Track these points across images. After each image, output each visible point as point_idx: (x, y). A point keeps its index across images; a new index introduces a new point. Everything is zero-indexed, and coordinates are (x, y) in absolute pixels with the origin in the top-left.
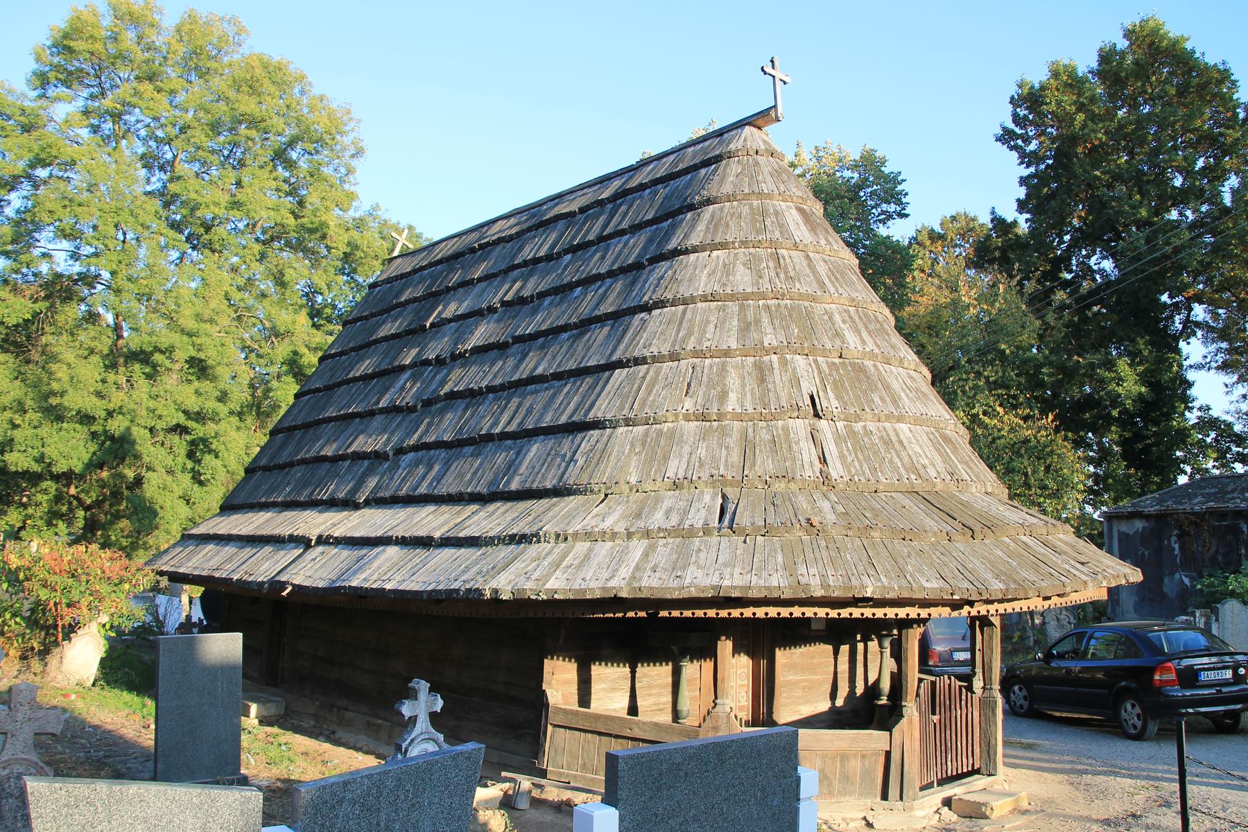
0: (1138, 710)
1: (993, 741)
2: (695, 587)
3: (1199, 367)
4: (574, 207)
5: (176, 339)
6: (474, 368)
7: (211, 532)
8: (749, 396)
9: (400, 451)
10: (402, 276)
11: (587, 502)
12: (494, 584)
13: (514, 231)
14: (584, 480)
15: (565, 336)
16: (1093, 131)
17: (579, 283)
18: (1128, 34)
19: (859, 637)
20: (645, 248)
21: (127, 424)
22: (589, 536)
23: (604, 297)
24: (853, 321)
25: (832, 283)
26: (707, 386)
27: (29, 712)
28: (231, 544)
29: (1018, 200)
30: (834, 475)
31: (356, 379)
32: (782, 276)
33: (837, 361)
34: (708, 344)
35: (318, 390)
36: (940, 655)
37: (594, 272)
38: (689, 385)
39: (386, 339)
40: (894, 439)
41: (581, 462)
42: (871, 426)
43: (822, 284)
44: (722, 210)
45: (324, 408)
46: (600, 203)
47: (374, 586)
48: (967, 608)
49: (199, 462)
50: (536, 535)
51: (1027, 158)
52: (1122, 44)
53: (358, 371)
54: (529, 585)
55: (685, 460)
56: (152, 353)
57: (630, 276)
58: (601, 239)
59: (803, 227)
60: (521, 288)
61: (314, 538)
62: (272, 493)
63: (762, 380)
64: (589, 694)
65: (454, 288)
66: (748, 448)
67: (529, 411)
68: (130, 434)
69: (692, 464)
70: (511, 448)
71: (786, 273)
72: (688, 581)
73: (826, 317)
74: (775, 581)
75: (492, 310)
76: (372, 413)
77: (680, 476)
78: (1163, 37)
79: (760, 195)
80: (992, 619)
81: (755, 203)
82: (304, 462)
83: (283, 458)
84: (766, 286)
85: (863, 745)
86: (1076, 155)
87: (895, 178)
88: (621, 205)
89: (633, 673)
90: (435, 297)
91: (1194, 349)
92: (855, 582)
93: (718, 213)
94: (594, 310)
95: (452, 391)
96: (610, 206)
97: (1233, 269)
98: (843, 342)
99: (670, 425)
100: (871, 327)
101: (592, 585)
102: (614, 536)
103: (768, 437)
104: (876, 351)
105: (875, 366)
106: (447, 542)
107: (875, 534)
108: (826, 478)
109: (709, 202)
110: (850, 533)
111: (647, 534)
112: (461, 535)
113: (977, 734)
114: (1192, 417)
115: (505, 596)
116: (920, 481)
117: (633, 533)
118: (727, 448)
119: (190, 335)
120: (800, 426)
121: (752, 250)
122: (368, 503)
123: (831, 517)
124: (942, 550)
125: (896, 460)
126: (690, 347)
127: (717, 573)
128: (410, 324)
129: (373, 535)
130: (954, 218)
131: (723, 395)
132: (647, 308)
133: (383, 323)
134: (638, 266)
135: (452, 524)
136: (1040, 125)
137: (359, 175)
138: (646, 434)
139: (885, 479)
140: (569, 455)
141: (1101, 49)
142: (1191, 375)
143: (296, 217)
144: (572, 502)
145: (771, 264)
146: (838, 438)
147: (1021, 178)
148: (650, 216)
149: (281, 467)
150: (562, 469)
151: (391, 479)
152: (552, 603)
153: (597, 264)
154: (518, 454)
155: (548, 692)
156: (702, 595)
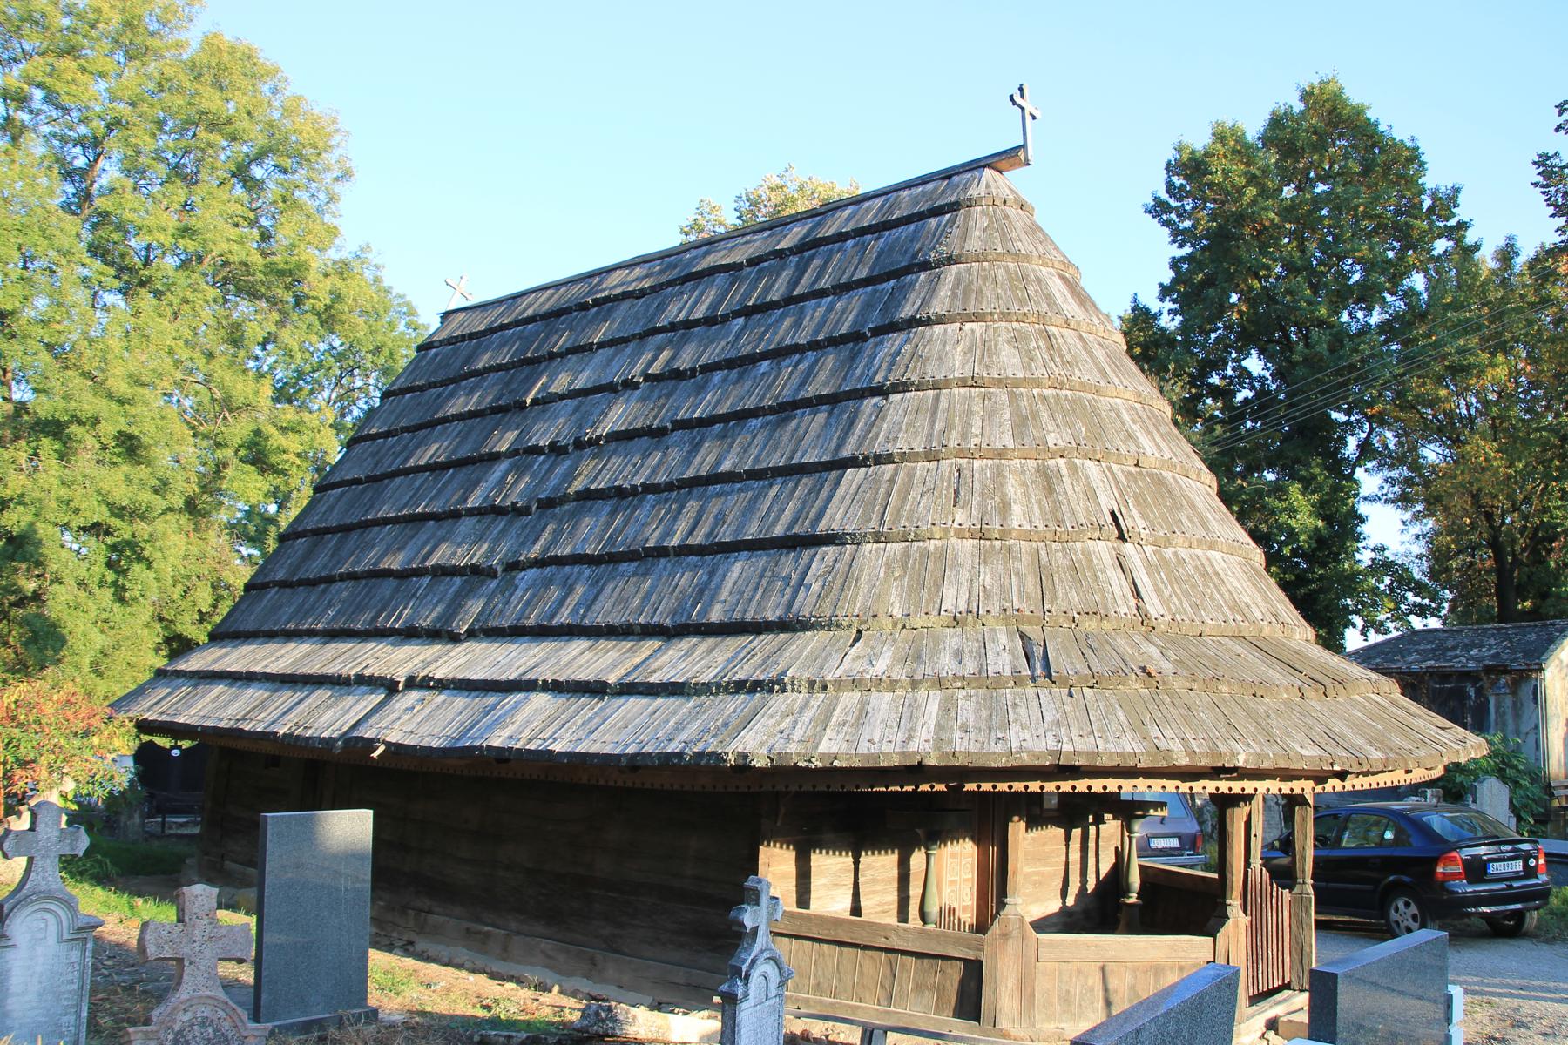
0: (1414, 909)
1: (1307, 949)
2: (1028, 752)
3: (1374, 499)
4: (739, 256)
5: (101, 406)
6: (616, 461)
7: (217, 667)
9: (513, 566)
10: (472, 336)
13: (646, 284)
14: (826, 610)
16: (1265, 209)
17: (764, 356)
18: (1306, 96)
19: (1091, 819)
20: (861, 314)
21: (30, 518)
22: (857, 684)
23: (808, 376)
26: (982, 494)
27: (209, 929)
28: (254, 684)
29: (1161, 285)
30: (1153, 613)
31: (418, 469)
32: (1057, 359)
33: (1133, 469)
34: (977, 440)
35: (357, 482)
37: (787, 342)
38: (957, 492)
39: (460, 417)
41: (816, 587)
42: (1183, 553)
43: (1103, 373)
44: (969, 270)
46: (780, 254)
47: (532, 746)
49: (125, 572)
51: (1179, 237)
52: (1298, 107)
53: (425, 456)
54: (792, 748)
55: (965, 588)
56: (67, 424)
58: (789, 300)
60: (673, 358)
62: (305, 617)
63: (1050, 490)
64: (808, 892)
66: (1043, 574)
67: (720, 519)
68: (35, 532)
69: (975, 593)
70: (696, 567)
71: (1061, 356)
72: (1015, 744)
75: (629, 385)
76: (455, 515)
77: (962, 607)
78: (1345, 104)
79: (1016, 255)
81: (1011, 265)
82: (352, 576)
83: (314, 569)
84: (1040, 372)
85: (1182, 954)
88: (812, 258)
89: (856, 863)
91: (1369, 480)
92: (1223, 748)
97: (1424, 384)
99: (938, 543)
100: (1162, 429)
101: (887, 748)
102: (893, 685)
103: (1067, 562)
106: (628, 689)
107: (1224, 688)
109: (950, 260)
111: (939, 683)
112: (652, 680)
113: (1287, 940)
114: (1365, 558)
115: (759, 763)
117: (920, 682)
118: (1018, 574)
119: (121, 402)
120: (1103, 550)
121: (1015, 325)
122: (471, 634)
125: (1217, 596)
126: (953, 444)
127: (1050, 735)
129: (503, 678)
131: (1005, 507)
132: (882, 391)
133: (452, 395)
135: (628, 665)
137: (343, 206)
138: (906, 553)
139: (1211, 620)
140: (795, 578)
141: (1274, 112)
142: (1363, 508)
143: (264, 254)
144: (809, 642)
145: (1042, 344)
146: (1150, 568)
148: (863, 274)
149: (311, 583)
150: (787, 597)
151: (507, 602)
152: (830, 772)
153: (784, 331)
154: (712, 574)
156: (1037, 763)
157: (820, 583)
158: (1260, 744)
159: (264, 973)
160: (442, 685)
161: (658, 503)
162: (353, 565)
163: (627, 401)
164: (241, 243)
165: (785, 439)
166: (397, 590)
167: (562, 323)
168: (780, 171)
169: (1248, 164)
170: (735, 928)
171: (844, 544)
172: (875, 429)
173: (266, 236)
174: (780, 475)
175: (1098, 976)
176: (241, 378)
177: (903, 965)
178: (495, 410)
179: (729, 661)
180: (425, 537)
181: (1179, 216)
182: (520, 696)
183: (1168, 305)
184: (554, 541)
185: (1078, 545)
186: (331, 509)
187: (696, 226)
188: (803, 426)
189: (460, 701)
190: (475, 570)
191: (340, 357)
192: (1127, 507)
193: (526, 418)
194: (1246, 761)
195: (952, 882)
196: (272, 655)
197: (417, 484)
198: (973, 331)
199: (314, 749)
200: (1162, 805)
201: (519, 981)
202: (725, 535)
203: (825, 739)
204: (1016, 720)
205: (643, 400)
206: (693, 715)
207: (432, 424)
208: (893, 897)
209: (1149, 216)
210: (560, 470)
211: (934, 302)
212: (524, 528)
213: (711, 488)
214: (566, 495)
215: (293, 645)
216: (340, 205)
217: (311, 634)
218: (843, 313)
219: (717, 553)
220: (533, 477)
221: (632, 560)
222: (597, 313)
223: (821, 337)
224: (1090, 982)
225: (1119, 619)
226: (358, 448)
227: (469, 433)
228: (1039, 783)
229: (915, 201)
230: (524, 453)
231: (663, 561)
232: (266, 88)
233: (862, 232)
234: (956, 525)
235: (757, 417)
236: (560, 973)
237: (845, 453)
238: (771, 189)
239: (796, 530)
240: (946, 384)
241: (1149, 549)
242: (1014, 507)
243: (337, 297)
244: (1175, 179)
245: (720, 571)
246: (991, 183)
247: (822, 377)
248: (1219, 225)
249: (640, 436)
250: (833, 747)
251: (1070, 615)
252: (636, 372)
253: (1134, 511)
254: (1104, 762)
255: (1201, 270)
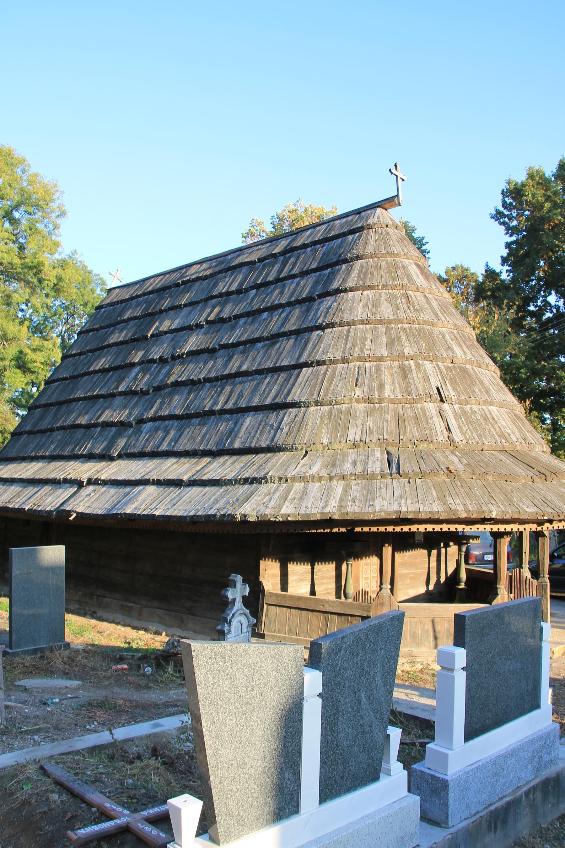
1: (545, 610)
2: (384, 512)
6: (191, 366)
8: (398, 387)
9: (141, 421)
10: (122, 301)
11: (293, 457)
12: (242, 511)
13: (208, 273)
14: (290, 441)
15: (260, 345)
19: (442, 545)
22: (302, 478)
23: (286, 319)
24: (457, 339)
25: (443, 314)
26: (370, 380)
29: (502, 257)
30: (457, 439)
31: (95, 372)
32: (412, 309)
33: (450, 365)
34: (368, 352)
35: (65, 379)
36: (476, 556)
37: (276, 302)
39: (116, 344)
40: (489, 416)
41: (286, 430)
42: (475, 408)
43: (436, 315)
44: (367, 263)
45: (73, 391)
46: (274, 256)
47: (145, 513)
48: (547, 525)
50: (265, 478)
51: (511, 231)
54: (268, 511)
55: (359, 428)
57: (305, 306)
58: (278, 280)
59: (421, 277)
60: (220, 312)
61: (85, 480)
63: (405, 377)
65: (166, 311)
66: (400, 420)
67: (240, 396)
69: (364, 431)
70: (229, 420)
71: (414, 307)
72: (378, 508)
73: (441, 336)
74: (435, 508)
75: (199, 326)
76: (113, 395)
77: (358, 438)
79: (392, 254)
80: (545, 532)
81: (389, 259)
82: (63, 428)
83: (44, 425)
84: (402, 315)
86: (543, 230)
87: (421, 241)
89: (313, 569)
90: (151, 316)
92: (484, 508)
93: (365, 265)
94: (281, 328)
95: (177, 381)
96: (281, 258)
98: (453, 353)
99: (347, 406)
100: (468, 343)
101: (314, 511)
102: (320, 479)
104: (473, 359)
105: (472, 369)
106: (193, 483)
107: (490, 478)
108: (451, 440)
109: (358, 258)
110: (474, 477)
111: (343, 477)
112: (204, 478)
115: (252, 519)
116: (507, 444)
117: (334, 477)
118: (387, 421)
120: (432, 407)
121: (390, 291)
122: (120, 456)
123: (460, 467)
124: (530, 488)
125: (492, 430)
126: (356, 354)
127: (396, 503)
128: (134, 334)
129: (133, 478)
130: (454, 269)
131: (381, 387)
132: (321, 328)
133: (112, 333)
134: (310, 299)
135: (194, 471)
136: (520, 208)
137: (62, 230)
138: (331, 411)
140: (276, 425)
141: (561, 161)
143: (21, 258)
144: (282, 457)
145: (404, 301)
146: (456, 416)
147: (507, 243)
148: (314, 266)
149: (43, 432)
150: (272, 434)
151: (137, 440)
152: (286, 523)
153: (276, 296)
154: (236, 424)
155: (264, 583)
156: (389, 517)
157: (288, 427)
158: (505, 506)
159: (13, 626)
160: (105, 483)
161: (211, 387)
162: (63, 422)
163: (197, 335)
164: (8, 253)
165: (274, 353)
166: (84, 435)
167: (166, 294)
168: (295, 202)
169: (546, 190)
170: (225, 599)
171: (300, 407)
172: (317, 348)
173: (22, 248)
174: (270, 372)
175: (430, 625)
176: (12, 323)
177: (332, 619)
178: (133, 340)
179: (242, 468)
180: (98, 407)
181: (509, 219)
182: (141, 487)
183: (506, 268)
184: (160, 408)
185: (419, 405)
186: (53, 393)
187: (250, 234)
188: (282, 346)
189: (113, 491)
190: (122, 424)
191: (66, 308)
192: (446, 385)
193: (148, 344)
194: (496, 515)
195: (366, 578)
196: (23, 469)
197: (95, 379)
198: (368, 295)
199: (43, 516)
200: (477, 537)
201: (146, 630)
202: (243, 404)
203: (285, 506)
204: (380, 496)
205: (206, 333)
206: (222, 496)
207: (103, 348)
208: (333, 586)
209: (493, 220)
210: (164, 371)
211: (349, 280)
212: (146, 401)
213: (237, 379)
214: (167, 384)
215: (34, 463)
216: (60, 230)
217: (43, 458)
218: (304, 286)
219: (239, 413)
220: (151, 375)
221: (198, 417)
222: (184, 288)
223: (293, 299)
224: (426, 627)
225: (438, 443)
226: (66, 361)
227: (120, 352)
228: (392, 527)
229: (342, 226)
230: (147, 362)
231: (213, 417)
232: (19, 170)
233: (315, 243)
234: (356, 396)
235: (260, 342)
236: (166, 625)
237: (302, 360)
238: (290, 212)
239: (277, 401)
240: (354, 323)
241: (456, 407)
242: (386, 386)
243: (60, 279)
244: (506, 199)
245: (240, 422)
246: (381, 216)
247: (293, 320)
248: (531, 224)
249: (203, 353)
250: (289, 511)
251: (413, 441)
252: (202, 320)
253: (449, 387)
254: (422, 516)
255: (523, 249)
